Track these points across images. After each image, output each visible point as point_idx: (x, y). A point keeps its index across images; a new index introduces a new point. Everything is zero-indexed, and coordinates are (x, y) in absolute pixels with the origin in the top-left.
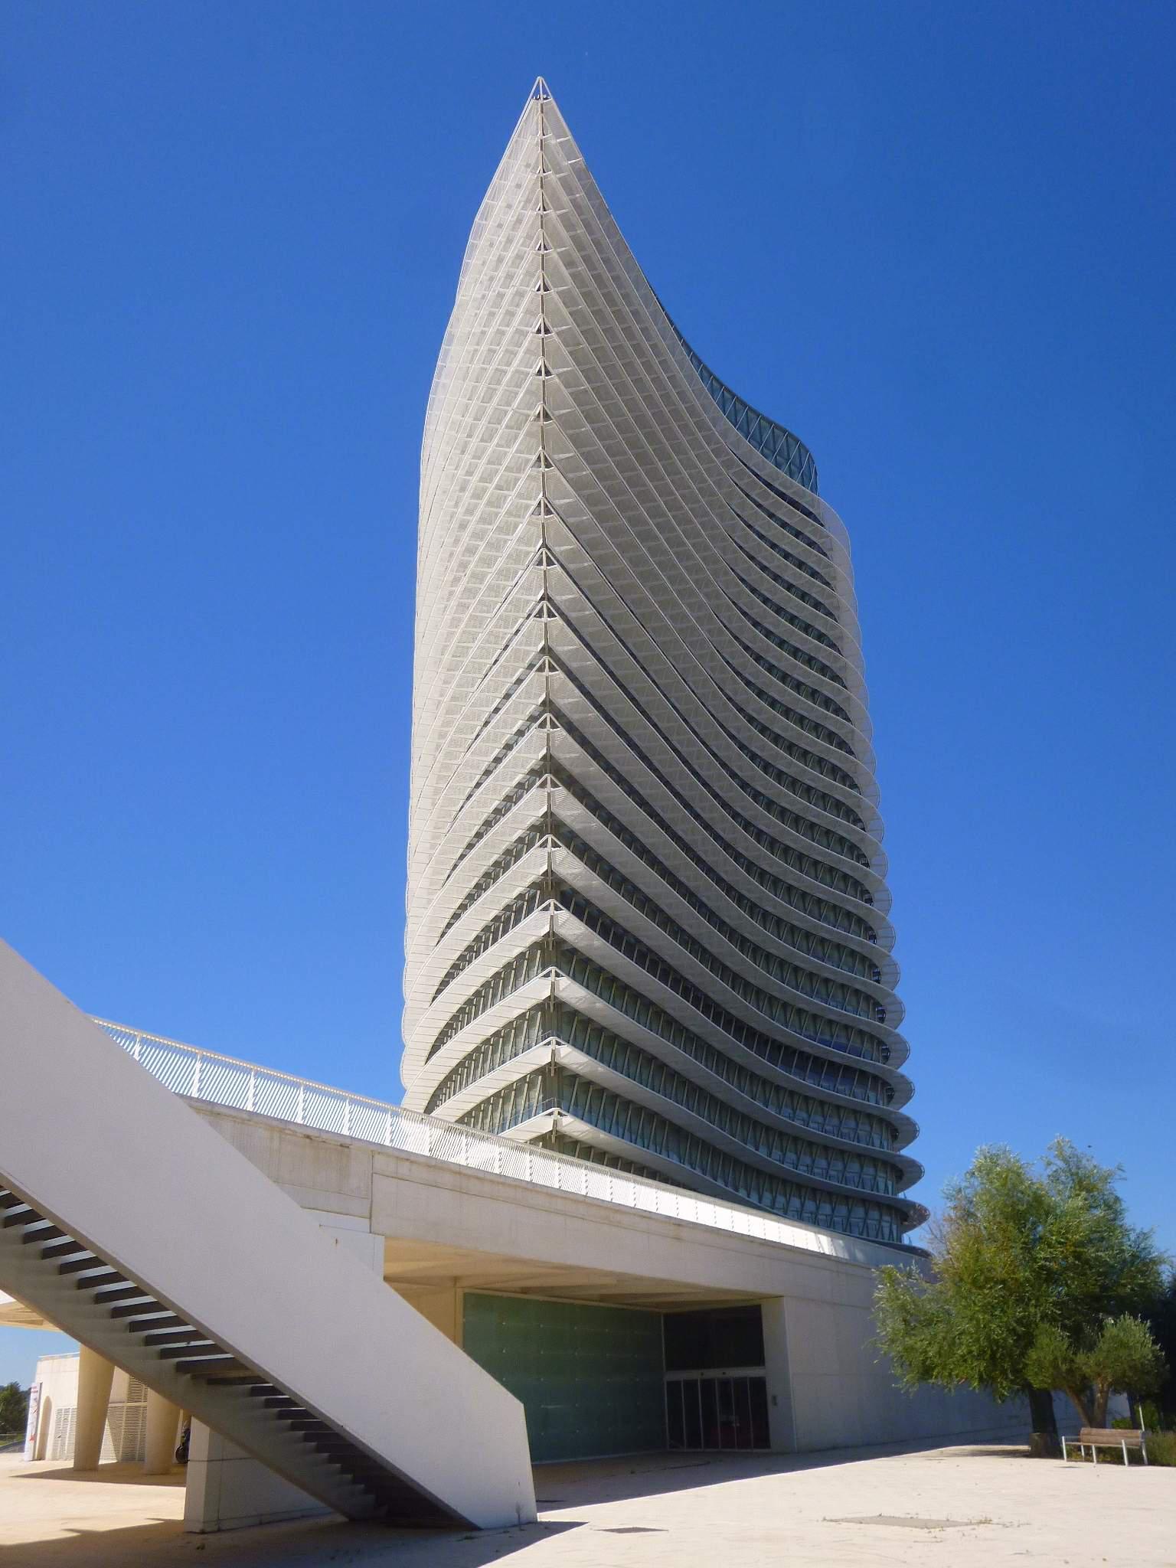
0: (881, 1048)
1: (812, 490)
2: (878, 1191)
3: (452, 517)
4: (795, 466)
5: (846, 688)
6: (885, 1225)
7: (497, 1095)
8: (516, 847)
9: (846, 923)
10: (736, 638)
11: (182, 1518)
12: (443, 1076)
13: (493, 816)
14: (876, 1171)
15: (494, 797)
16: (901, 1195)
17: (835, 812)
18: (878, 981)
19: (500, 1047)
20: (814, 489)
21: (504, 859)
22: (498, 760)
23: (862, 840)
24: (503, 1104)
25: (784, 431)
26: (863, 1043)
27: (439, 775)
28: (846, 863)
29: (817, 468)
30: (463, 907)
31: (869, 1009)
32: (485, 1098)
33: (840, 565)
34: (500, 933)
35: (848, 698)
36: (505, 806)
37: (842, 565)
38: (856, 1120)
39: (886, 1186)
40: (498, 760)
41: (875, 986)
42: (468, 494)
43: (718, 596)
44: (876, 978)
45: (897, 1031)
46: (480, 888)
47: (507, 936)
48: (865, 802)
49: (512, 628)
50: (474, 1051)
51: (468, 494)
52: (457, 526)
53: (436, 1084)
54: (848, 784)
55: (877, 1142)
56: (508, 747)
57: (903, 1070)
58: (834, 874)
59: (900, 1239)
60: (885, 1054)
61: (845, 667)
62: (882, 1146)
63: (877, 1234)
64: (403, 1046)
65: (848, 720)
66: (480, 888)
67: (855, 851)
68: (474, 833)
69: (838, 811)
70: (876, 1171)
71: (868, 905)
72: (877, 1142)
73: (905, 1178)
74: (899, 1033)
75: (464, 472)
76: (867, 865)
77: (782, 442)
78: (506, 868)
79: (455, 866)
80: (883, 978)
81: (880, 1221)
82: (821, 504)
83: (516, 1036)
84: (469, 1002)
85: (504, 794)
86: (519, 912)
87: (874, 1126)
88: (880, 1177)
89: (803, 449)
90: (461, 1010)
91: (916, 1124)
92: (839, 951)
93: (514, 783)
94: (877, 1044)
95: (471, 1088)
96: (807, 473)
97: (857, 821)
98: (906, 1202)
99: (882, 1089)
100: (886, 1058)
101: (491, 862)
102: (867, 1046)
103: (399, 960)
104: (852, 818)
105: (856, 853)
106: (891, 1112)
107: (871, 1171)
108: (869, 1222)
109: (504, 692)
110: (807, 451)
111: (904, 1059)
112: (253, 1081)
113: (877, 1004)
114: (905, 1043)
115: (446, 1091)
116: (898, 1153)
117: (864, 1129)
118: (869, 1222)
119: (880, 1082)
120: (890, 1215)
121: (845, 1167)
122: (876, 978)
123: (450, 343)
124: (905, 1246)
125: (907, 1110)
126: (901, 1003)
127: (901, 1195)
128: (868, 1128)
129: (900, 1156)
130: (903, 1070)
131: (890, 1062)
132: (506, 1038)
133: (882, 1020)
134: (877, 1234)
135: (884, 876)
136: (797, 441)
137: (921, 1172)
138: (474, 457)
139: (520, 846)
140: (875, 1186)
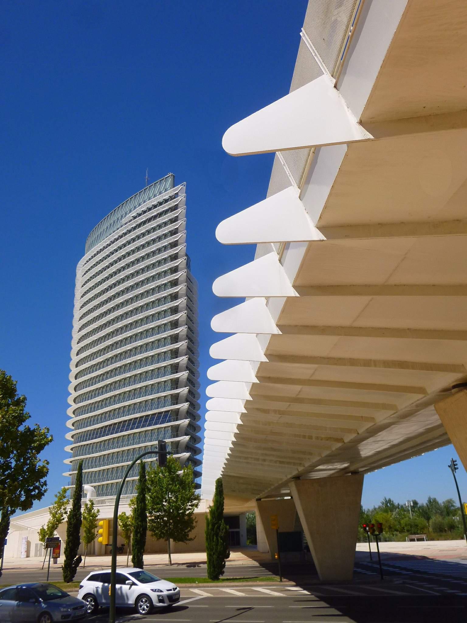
16: (195, 457)
23: (193, 316)
45: (197, 412)
74: (198, 424)
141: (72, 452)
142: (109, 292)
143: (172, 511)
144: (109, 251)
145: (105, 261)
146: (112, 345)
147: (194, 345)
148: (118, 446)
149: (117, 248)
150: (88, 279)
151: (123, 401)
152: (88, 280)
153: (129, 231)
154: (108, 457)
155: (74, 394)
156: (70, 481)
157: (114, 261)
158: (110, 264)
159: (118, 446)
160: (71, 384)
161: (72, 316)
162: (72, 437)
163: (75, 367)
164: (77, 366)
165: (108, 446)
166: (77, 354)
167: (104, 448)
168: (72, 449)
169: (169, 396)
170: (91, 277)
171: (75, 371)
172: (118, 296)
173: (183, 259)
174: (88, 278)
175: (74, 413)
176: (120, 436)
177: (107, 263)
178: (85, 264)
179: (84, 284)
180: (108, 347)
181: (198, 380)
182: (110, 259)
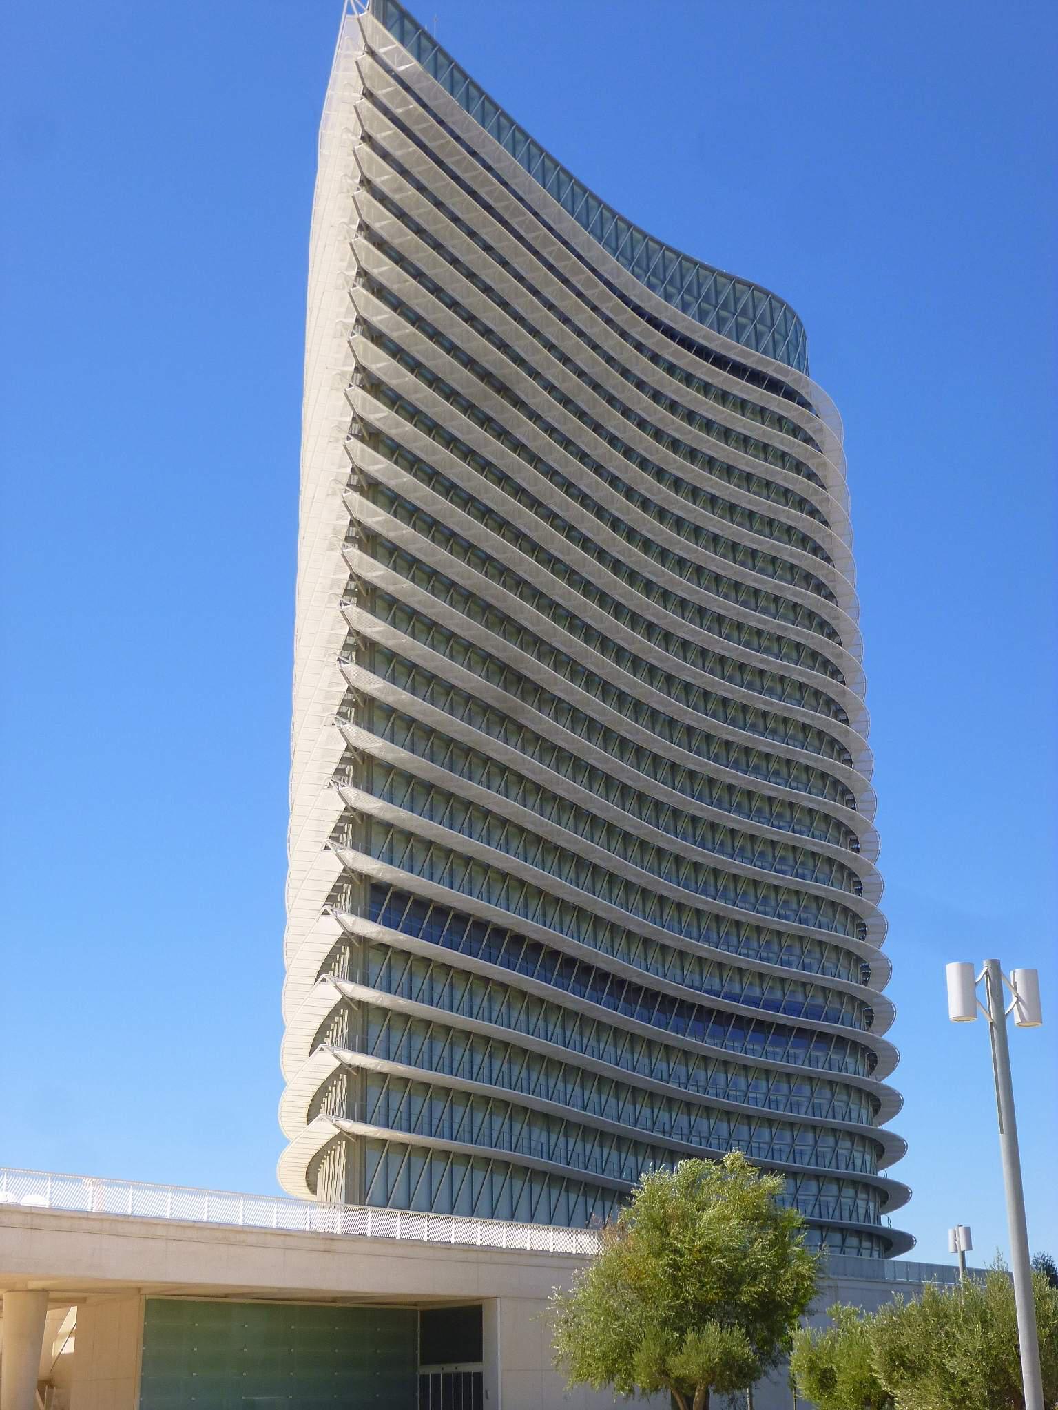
0: (856, 923)
4: (780, 334)
5: (824, 488)
6: (861, 1204)
9: (813, 702)
11: (72, 1351)
14: (853, 1145)
16: (880, 1174)
17: (804, 585)
18: (857, 850)
20: (807, 374)
25: (767, 293)
26: (842, 1004)
28: (809, 598)
29: (806, 333)
33: (840, 536)
35: (824, 464)
38: (832, 1089)
39: (863, 1163)
45: (882, 993)
48: (846, 655)
53: (326, 1012)
57: (886, 1037)
61: (820, 430)
62: (860, 1119)
67: (840, 751)
69: (811, 623)
70: (853, 1145)
73: (885, 1156)
76: (846, 721)
77: (764, 306)
88: (857, 1151)
89: (789, 312)
92: (811, 816)
96: (794, 342)
97: (833, 634)
99: (863, 1056)
102: (846, 1008)
103: (283, 812)
104: (826, 630)
105: (833, 707)
107: (848, 1144)
108: (843, 1200)
112: (49, 1183)
115: (344, 1012)
117: (840, 1099)
118: (843, 1200)
119: (847, 871)
121: (819, 1191)
125: (890, 1081)
127: (880, 1174)
128: (845, 1098)
130: (886, 1037)
133: (860, 892)
134: (851, 1216)
135: (875, 861)
136: (782, 303)
140: (850, 1162)
147: (846, 721)
161: (278, 1028)
163: (305, 1120)
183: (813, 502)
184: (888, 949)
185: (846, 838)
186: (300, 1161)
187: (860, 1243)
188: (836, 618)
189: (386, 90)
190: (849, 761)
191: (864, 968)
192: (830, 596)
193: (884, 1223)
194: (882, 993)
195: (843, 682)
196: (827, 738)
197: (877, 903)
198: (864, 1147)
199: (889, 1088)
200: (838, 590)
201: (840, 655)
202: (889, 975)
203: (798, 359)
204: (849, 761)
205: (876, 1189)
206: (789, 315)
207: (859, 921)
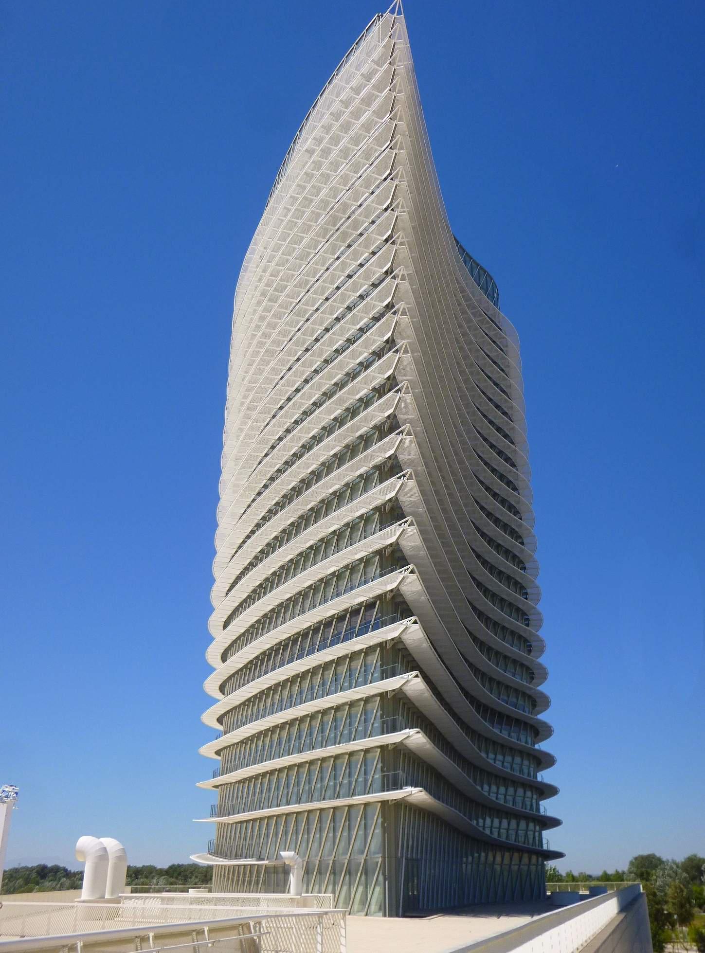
1: (494, 304)
2: (523, 775)
3: (256, 287)
7: (269, 689)
8: (289, 528)
10: (483, 392)
12: (238, 604)
13: (273, 541)
15: (276, 495)
16: (537, 746)
19: (273, 657)
21: (281, 535)
22: (280, 439)
24: (273, 694)
27: (251, 360)
30: (253, 532)
31: (518, 617)
32: (261, 690)
34: (277, 547)
35: (513, 428)
36: (284, 468)
37: (514, 359)
40: (280, 439)
41: (523, 601)
42: (268, 274)
43: (474, 308)
44: (525, 597)
45: (537, 633)
46: (265, 519)
47: (281, 549)
49: (295, 328)
50: (255, 658)
51: (268, 274)
52: (258, 318)
54: (511, 487)
55: (523, 739)
56: (288, 431)
58: (505, 631)
59: (536, 777)
60: (529, 649)
61: (512, 407)
63: (522, 806)
64: (215, 553)
65: (512, 443)
66: (265, 519)
68: (262, 485)
71: (522, 572)
72: (523, 739)
75: (264, 285)
78: (283, 507)
79: (249, 506)
80: (529, 597)
81: (522, 764)
82: (502, 316)
83: (285, 612)
84: (254, 591)
85: (284, 460)
86: (289, 535)
87: (520, 698)
90: (249, 597)
91: (546, 668)
93: (290, 487)
94: (524, 642)
95: (254, 643)
97: (516, 513)
98: (538, 690)
100: (530, 651)
101: (274, 502)
103: (213, 525)
106: (532, 689)
109: (287, 396)
110: (492, 279)
111: (542, 651)
113: (524, 614)
114: (545, 669)
116: (535, 717)
119: (519, 586)
120: (529, 760)
122: (525, 597)
123: (245, 272)
124: (539, 803)
125: (542, 717)
126: (542, 641)
127: (537, 746)
129: (537, 719)
131: (532, 654)
132: (278, 613)
137: (552, 731)
138: (271, 275)
139: (293, 493)
141: (219, 758)
142: (335, 473)
143: (410, 894)
144: (369, 249)
145: (318, 447)
146: (338, 575)
147: (522, 543)
148: (366, 729)
149: (340, 451)
150: (278, 469)
151: (346, 684)
152: (279, 471)
153: (352, 376)
154: (334, 767)
155: (223, 670)
156: (216, 801)
157: (361, 398)
158: (347, 409)
159: (366, 729)
160: (214, 673)
161: (211, 581)
162: (220, 720)
163: (222, 628)
164: (224, 658)
165: (350, 725)
166: (226, 625)
167: (335, 734)
168: (218, 753)
169: (376, 749)
170: (270, 511)
171: (222, 639)
172: (351, 494)
173: (407, 569)
174: (263, 514)
175: (222, 689)
176: (339, 755)
177: (337, 374)
178: (266, 455)
179: (230, 590)
180: (325, 582)
181: (537, 607)
182: (348, 393)
183: (507, 453)
184: (540, 607)
185: (521, 590)
186: (217, 711)
187: (522, 761)
188: (518, 503)
189: (280, 621)
190: (524, 568)
191: (528, 644)
192: (515, 489)
193: (539, 779)
194: (537, 633)
195: (521, 519)
196: (515, 607)
197: (536, 605)
198: (525, 702)
199: (542, 693)
200: (518, 462)
201: (520, 526)
202: (546, 679)
203: (493, 285)
204: (524, 568)
205: (532, 727)
206: (489, 279)
207: (528, 644)
